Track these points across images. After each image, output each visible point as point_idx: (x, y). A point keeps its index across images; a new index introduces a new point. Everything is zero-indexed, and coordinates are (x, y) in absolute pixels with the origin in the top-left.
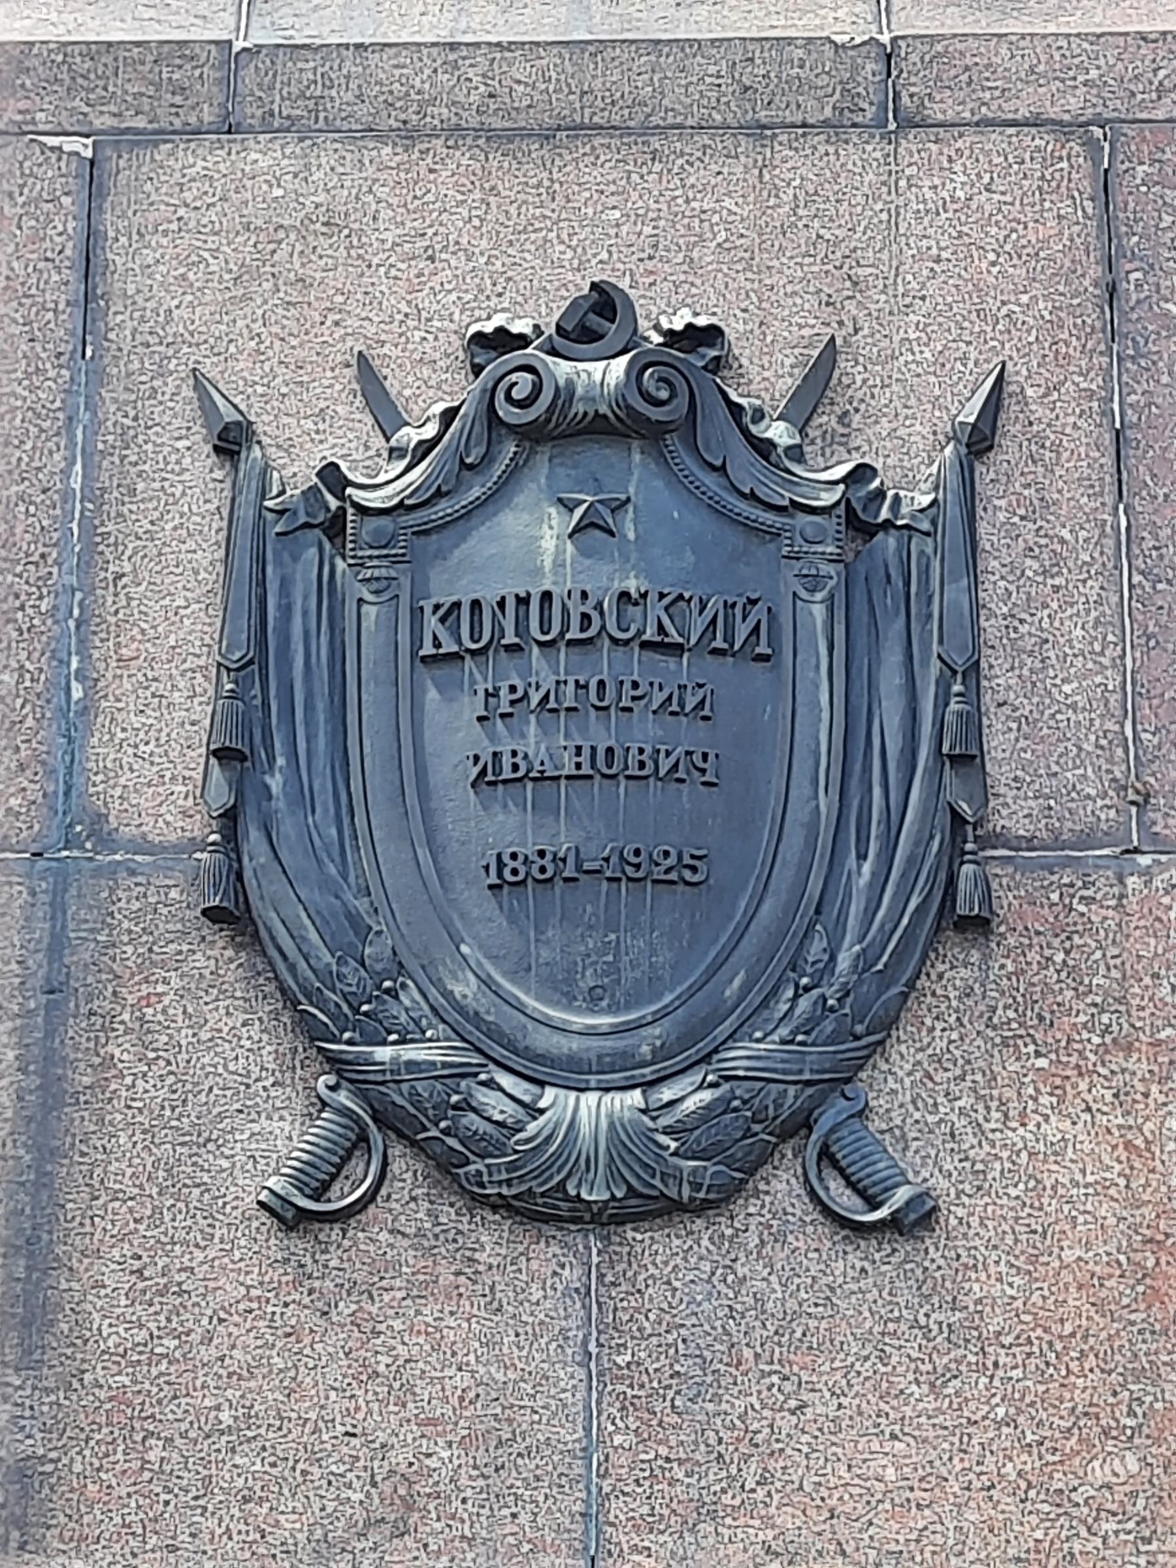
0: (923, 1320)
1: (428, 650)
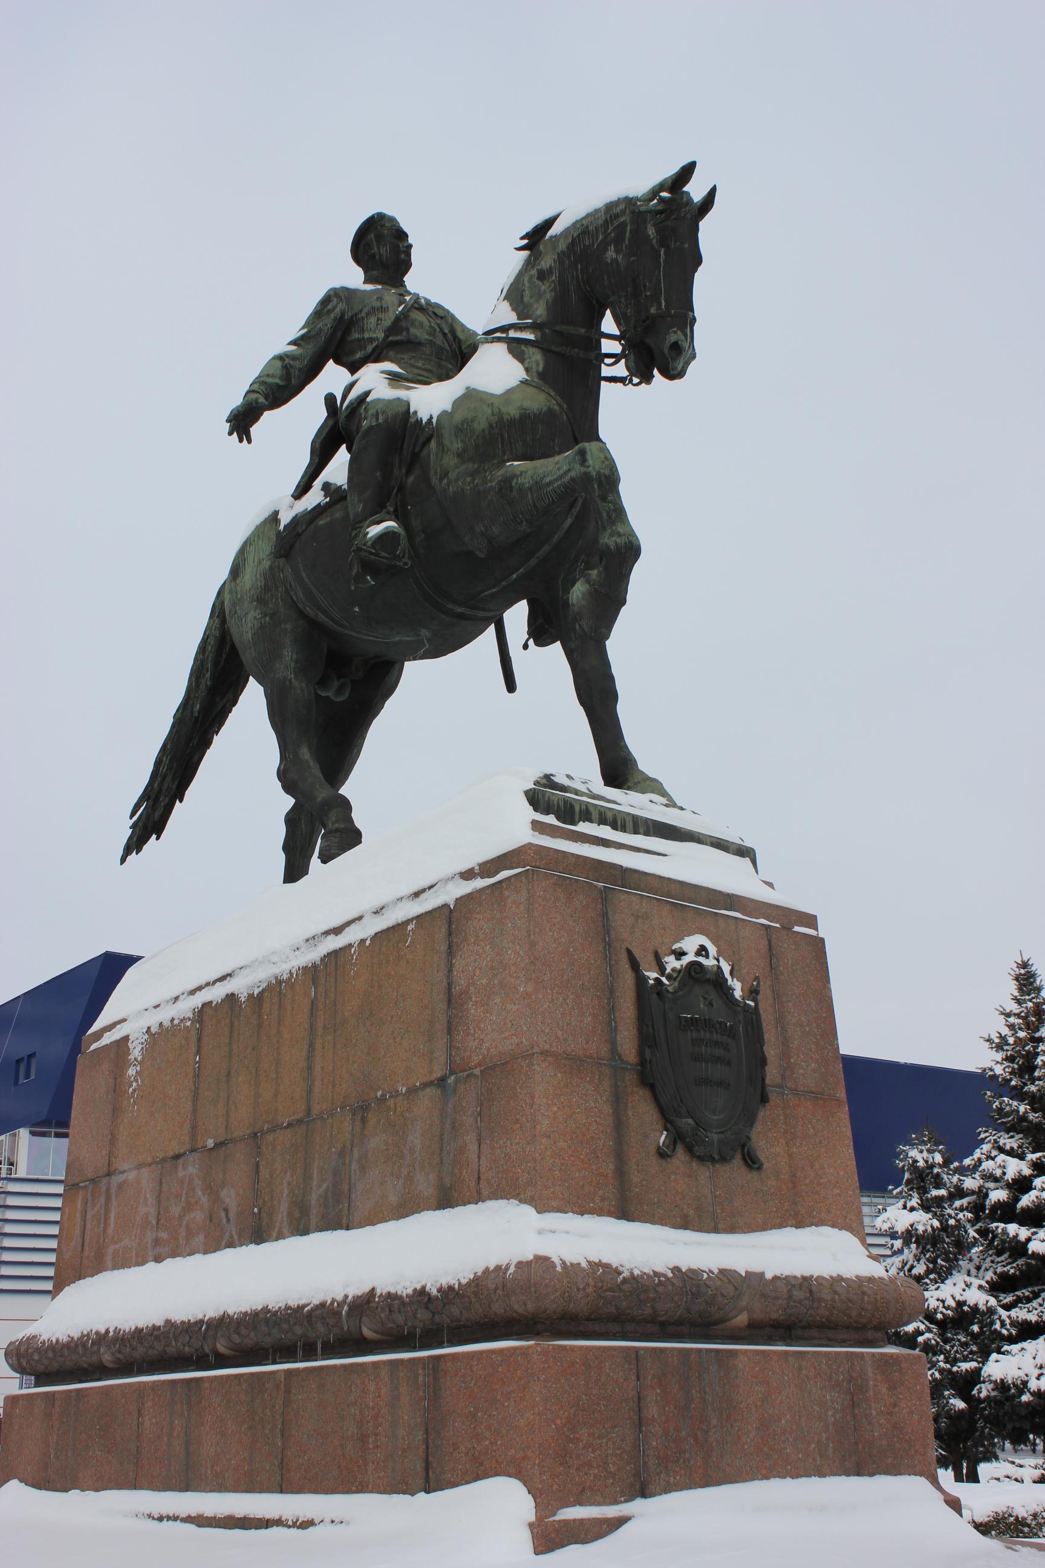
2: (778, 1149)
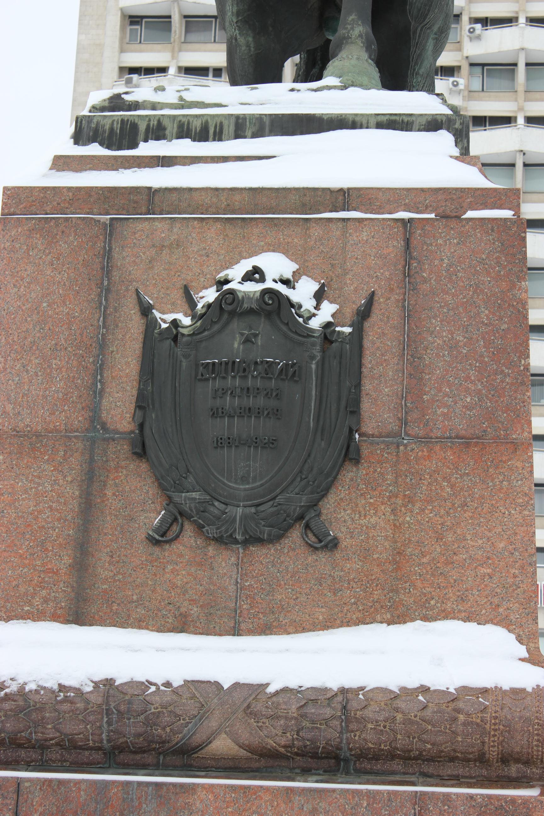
0: (332, 574)
1: (199, 377)
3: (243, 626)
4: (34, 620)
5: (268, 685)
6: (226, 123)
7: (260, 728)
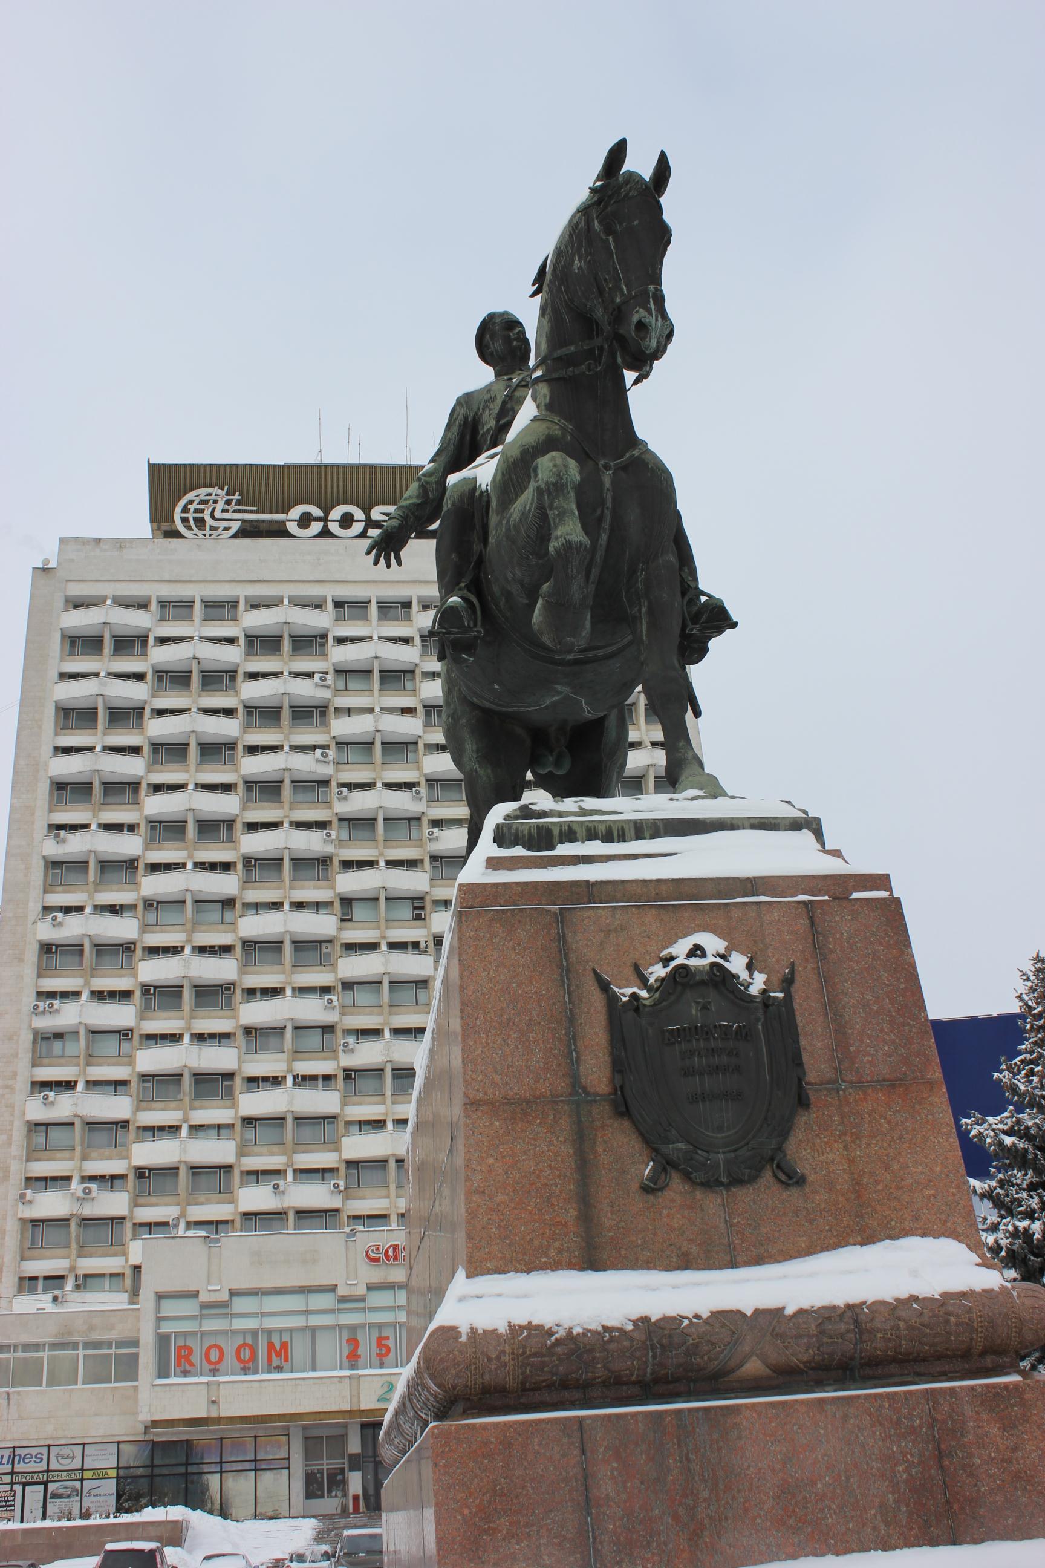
2: (830, 1157)
3: (739, 1259)
4: (553, 1270)
5: (783, 1308)
6: (626, 828)
7: (786, 1347)
